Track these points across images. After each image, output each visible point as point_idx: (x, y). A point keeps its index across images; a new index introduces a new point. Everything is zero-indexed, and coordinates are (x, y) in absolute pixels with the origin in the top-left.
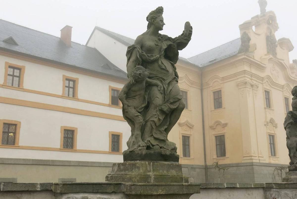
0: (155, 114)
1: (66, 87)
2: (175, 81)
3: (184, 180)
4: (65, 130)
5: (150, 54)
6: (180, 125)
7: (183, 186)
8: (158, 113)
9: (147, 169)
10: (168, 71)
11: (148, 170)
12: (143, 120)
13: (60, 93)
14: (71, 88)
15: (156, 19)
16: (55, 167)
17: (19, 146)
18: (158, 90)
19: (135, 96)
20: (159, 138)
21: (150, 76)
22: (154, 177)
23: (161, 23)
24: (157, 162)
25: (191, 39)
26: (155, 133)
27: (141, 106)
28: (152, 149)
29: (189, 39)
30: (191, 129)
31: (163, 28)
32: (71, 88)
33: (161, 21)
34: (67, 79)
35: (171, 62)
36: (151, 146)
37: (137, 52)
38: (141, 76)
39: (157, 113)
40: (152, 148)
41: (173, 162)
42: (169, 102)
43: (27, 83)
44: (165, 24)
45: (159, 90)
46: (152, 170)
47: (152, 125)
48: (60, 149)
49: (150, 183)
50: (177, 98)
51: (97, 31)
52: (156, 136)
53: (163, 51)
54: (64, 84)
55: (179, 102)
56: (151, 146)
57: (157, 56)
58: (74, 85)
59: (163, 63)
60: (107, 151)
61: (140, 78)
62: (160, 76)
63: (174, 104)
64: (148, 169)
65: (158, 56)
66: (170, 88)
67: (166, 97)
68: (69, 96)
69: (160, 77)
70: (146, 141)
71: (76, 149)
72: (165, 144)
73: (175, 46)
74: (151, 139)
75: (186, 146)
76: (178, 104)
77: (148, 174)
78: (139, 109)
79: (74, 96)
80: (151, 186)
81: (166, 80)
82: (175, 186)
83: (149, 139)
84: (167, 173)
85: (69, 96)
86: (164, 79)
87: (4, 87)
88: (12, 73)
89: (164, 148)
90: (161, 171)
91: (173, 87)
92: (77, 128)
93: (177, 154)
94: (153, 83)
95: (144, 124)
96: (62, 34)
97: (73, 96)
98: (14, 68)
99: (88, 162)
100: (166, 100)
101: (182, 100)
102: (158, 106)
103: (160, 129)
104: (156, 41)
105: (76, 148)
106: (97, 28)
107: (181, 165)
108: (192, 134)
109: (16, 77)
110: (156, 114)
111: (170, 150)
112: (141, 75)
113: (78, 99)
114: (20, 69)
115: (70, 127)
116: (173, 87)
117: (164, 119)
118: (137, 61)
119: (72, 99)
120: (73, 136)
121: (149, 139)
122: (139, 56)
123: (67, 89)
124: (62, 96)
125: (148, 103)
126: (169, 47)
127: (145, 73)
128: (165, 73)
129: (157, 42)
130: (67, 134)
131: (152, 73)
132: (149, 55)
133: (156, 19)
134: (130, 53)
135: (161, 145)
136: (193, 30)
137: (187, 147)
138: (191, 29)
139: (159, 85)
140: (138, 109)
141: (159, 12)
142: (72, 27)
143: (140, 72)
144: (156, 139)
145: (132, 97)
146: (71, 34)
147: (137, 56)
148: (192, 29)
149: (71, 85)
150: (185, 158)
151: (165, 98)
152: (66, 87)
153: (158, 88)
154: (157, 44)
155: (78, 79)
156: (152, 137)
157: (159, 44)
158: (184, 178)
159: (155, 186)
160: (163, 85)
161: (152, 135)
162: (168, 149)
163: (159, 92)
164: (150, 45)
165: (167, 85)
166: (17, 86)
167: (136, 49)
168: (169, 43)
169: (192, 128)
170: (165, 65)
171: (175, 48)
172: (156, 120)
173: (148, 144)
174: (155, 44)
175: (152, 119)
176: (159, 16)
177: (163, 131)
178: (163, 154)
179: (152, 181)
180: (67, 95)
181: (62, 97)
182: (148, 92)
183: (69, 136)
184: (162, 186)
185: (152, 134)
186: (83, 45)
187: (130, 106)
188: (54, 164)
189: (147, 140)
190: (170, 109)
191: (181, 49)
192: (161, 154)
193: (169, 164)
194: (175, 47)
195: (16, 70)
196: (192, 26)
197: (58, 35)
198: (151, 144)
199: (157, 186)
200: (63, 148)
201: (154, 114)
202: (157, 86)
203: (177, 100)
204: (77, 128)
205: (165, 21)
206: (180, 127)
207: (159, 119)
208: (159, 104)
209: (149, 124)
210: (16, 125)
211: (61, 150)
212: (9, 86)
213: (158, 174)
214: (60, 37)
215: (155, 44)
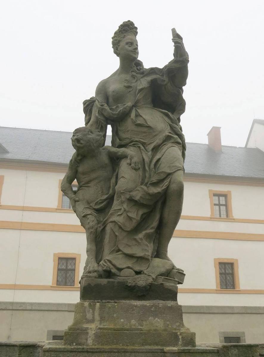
0: (119, 208)
1: (215, 205)
3: (181, 340)
4: (220, 263)
7: (164, 352)
8: (125, 206)
9: (86, 316)
11: (86, 319)
13: (208, 214)
15: (119, 44)
16: (212, 315)
17: (240, 291)
20: (134, 254)
22: (94, 334)
24: (116, 301)
28: (118, 276)
34: (215, 195)
35: (163, 111)
38: (81, 143)
41: (161, 302)
43: (236, 213)
46: (97, 317)
48: (216, 290)
49: (85, 347)
50: (163, 172)
51: (256, 125)
54: (211, 201)
55: (168, 180)
58: (226, 201)
60: (214, 289)
61: (82, 148)
62: (137, 139)
64: (89, 316)
68: (220, 216)
69: (136, 141)
71: (240, 289)
77: (85, 326)
79: (228, 217)
80: (71, 352)
82: (138, 352)
84: (137, 324)
85: (220, 216)
87: (212, 219)
88: (217, 203)
90: (122, 320)
91: (163, 155)
92: (237, 260)
95: (100, 229)
96: (210, 140)
97: (227, 216)
98: (219, 195)
99: (202, 307)
102: (122, 193)
103: (136, 238)
104: (126, 80)
105: (239, 288)
106: (255, 122)
107: (181, 306)
109: (222, 207)
113: (234, 219)
114: (225, 196)
115: (228, 259)
120: (233, 271)
123: (217, 207)
124: (211, 218)
126: (154, 84)
128: (145, 132)
130: (225, 269)
131: (126, 137)
133: (119, 44)
135: (137, 268)
140: (92, 205)
141: (124, 30)
142: (220, 128)
143: (77, 136)
144: (130, 256)
145: (84, 185)
146: (220, 137)
152: (215, 205)
155: (230, 192)
156: (120, 253)
157: (133, 85)
158: (180, 334)
159: (83, 352)
161: (119, 250)
163: (130, 167)
164: (113, 90)
165: (150, 153)
166: (225, 216)
170: (144, 119)
171: (166, 84)
175: (111, 220)
177: (141, 239)
178: (129, 285)
179: (90, 341)
180: (218, 216)
181: (211, 219)
183: (227, 271)
184: (100, 352)
187: (78, 201)
188: (211, 312)
190: (149, 194)
192: (127, 285)
193: (144, 306)
194: (165, 83)
195: (221, 198)
197: (205, 141)
198: (114, 266)
199: (87, 352)
200: (221, 289)
203: (163, 176)
204: (237, 260)
207: (130, 218)
208: (125, 188)
210: (74, 259)
211: (52, 288)
212: (217, 217)
213: (112, 326)
214: (207, 143)
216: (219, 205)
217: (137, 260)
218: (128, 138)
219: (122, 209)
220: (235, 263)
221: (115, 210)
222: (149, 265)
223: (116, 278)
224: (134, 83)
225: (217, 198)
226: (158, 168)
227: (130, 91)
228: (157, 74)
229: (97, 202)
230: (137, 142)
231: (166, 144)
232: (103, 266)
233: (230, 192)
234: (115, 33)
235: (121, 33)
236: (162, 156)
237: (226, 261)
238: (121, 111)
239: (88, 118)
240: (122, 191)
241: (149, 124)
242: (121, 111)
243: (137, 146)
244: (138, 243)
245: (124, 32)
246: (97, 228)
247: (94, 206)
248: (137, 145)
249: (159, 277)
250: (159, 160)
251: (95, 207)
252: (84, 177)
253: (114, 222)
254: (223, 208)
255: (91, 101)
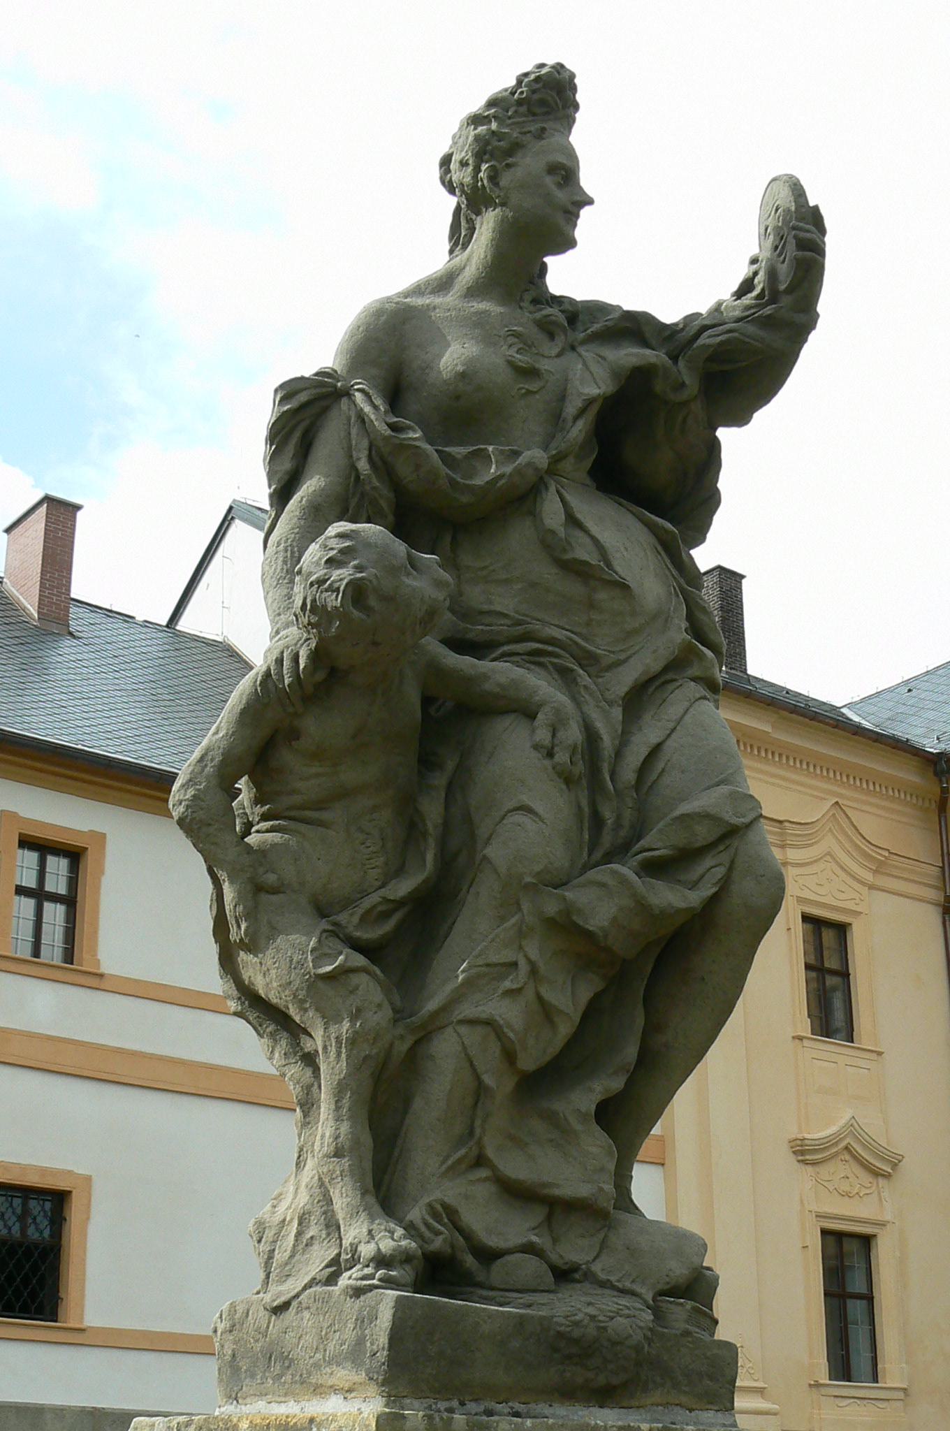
0: (507, 955)
1: (21, 891)
2: (694, 679)
5: (461, 443)
6: (802, 1153)
8: (533, 950)
10: (623, 587)
12: (390, 1013)
14: (55, 898)
15: (510, 160)
17: (82, 1330)
18: (536, 747)
19: (320, 805)
20: (545, 1185)
21: (470, 636)
23: (559, 186)
25: (818, 315)
26: (512, 1138)
27: (382, 892)
29: (800, 318)
30: (881, 1181)
31: (579, 233)
32: (55, 898)
33: (553, 169)
36: (469, 1261)
37: (354, 431)
39: (521, 947)
40: (481, 1277)
42: (640, 857)
44: (590, 202)
45: (547, 742)
47: (472, 1064)
52: (516, 1168)
53: (576, 418)
55: (725, 858)
56: (469, 1261)
57: (521, 460)
58: (73, 882)
59: (579, 516)
63: (683, 877)
65: (536, 456)
66: (648, 734)
67: (608, 814)
68: (36, 952)
70: (416, 1214)
72: (603, 1245)
73: (683, 385)
74: (467, 1197)
75: (850, 1303)
76: (720, 872)
78: (363, 919)
81: (610, 668)
83: (450, 1192)
85: (36, 952)
86: (588, 660)
88: (30, 881)
89: (589, 1277)
91: (673, 730)
92: (88, 1179)
93: (722, 1334)
94: (487, 686)
95: (403, 1047)
98: (41, 846)
100: (607, 840)
101: (752, 836)
104: (516, 335)
108: (888, 1217)
110: (514, 965)
111: (649, 1297)
112: (372, 602)
113: (101, 976)
114: (75, 856)
115: (44, 1171)
116: (673, 730)
117: (591, 1013)
118: (353, 502)
119: (58, 975)
121: (450, 1192)
122: (370, 459)
123: (28, 904)
125: (446, 863)
127: (408, 581)
129: (525, 344)
132: (458, 451)
134: (297, 434)
136: (827, 239)
137: (856, 1309)
138: (813, 229)
139: (540, 705)
140: (349, 920)
145: (308, 814)
147: (353, 467)
148: (822, 230)
149: (57, 882)
150: (844, 1389)
151: (597, 822)
152: (21, 891)
153: (533, 731)
154: (522, 359)
156: (483, 1173)
157: (544, 365)
160: (574, 698)
161: (480, 1161)
162: (628, 1285)
163: (547, 763)
165: (617, 713)
167: (344, 400)
168: (630, 355)
169: (887, 1176)
170: (593, 538)
171: (685, 404)
172: (510, 1013)
173: (437, 1244)
174: (511, 364)
175: (467, 1010)
176: (541, 134)
180: (25, 952)
182: (450, 765)
183: (31, 1231)
185: (480, 1143)
186: (147, 624)
187: (275, 891)
189: (426, 1200)
190: (642, 906)
191: (740, 418)
194: (684, 395)
196: (816, 208)
198: (467, 1235)
201: (494, 959)
202: (528, 713)
203: (703, 834)
205: (588, 180)
206: (810, 1169)
207: (547, 1012)
208: (537, 868)
209: (445, 1047)
215: (511, 364)
216: (39, 895)
217: (549, 1218)
218: (505, 616)
219: (522, 963)
220: (74, 1194)
221: (488, 965)
222: (603, 1241)
223: (471, 1293)
224: (549, 357)
225: (32, 857)
226: (651, 787)
227: (529, 392)
228: (645, 344)
229: (368, 912)
230: (552, 645)
231: (675, 680)
232: (427, 1234)
233: (101, 838)
234: (492, 103)
235: (523, 109)
236: (669, 735)
237: (33, 1180)
238: (503, 481)
239: (286, 465)
240: (528, 879)
241: (623, 575)
242: (503, 481)
243: (553, 664)
244: (562, 1133)
245: (538, 110)
246: (391, 1045)
247: (357, 927)
248: (556, 660)
249: (660, 1301)
250: (656, 750)
251: (358, 934)
252: (313, 770)
253: (488, 1023)
254: (55, 914)
255: (324, 390)
